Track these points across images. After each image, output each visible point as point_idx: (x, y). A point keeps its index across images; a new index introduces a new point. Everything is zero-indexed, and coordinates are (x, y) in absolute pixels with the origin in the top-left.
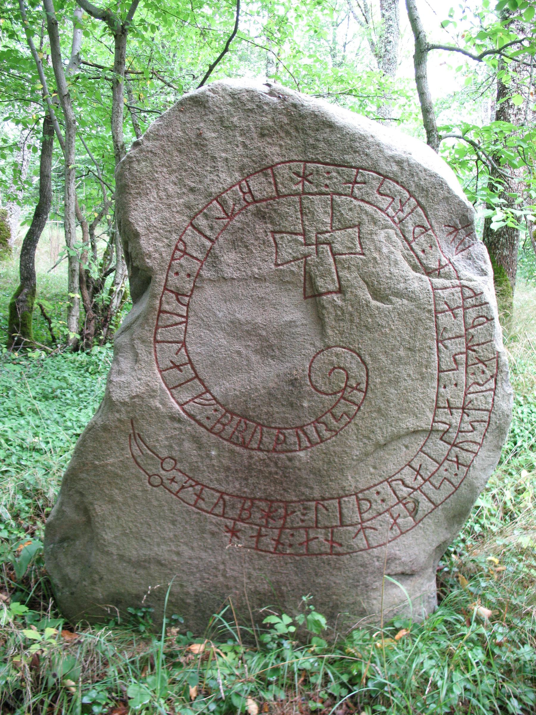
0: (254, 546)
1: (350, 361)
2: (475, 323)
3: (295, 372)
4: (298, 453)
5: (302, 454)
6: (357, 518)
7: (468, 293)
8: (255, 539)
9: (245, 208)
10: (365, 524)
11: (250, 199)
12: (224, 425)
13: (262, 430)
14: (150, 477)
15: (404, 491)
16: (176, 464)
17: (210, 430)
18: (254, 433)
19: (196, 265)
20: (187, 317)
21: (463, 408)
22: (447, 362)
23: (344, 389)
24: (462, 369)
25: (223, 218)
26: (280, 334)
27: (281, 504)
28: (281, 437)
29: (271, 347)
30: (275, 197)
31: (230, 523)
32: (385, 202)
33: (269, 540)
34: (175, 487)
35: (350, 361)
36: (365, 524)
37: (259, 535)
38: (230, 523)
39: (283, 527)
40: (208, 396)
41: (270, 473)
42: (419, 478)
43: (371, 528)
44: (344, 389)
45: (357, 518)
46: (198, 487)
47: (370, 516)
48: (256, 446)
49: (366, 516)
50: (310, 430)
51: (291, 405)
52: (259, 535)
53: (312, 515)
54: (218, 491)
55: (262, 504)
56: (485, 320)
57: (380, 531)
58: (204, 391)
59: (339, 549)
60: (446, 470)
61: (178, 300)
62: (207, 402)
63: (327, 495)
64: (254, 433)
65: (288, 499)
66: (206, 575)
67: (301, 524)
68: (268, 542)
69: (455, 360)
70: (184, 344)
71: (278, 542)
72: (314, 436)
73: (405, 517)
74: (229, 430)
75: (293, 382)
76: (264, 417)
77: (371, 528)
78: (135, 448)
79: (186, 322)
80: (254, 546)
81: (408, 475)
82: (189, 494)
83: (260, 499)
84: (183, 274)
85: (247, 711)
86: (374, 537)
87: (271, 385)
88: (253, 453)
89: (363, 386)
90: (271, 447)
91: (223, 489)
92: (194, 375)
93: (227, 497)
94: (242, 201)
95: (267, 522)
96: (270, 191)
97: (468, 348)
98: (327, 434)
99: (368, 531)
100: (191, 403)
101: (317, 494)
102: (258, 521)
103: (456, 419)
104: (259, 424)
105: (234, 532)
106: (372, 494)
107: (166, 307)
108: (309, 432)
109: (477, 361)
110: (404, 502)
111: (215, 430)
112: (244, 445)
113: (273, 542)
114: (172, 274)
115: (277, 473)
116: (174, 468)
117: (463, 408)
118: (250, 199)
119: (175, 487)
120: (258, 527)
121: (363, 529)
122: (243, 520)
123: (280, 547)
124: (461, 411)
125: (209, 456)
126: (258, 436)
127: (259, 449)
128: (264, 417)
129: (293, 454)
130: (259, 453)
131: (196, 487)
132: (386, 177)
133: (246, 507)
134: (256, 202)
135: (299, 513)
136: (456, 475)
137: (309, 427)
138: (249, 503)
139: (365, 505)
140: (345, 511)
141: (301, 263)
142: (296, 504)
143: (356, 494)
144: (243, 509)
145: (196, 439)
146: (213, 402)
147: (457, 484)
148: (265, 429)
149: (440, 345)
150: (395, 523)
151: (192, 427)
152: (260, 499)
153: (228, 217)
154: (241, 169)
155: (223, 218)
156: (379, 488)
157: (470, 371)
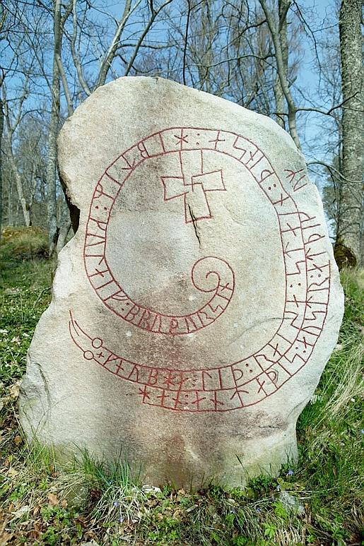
0: (160, 404)
3: (181, 276)
4: (188, 335)
5: (190, 335)
6: (232, 384)
7: (304, 217)
8: (161, 399)
9: (143, 161)
10: (239, 389)
11: (145, 155)
12: (134, 315)
13: (160, 317)
14: (85, 352)
15: (266, 364)
17: (125, 319)
18: (155, 320)
20: (105, 238)
21: (306, 302)
22: (292, 268)
25: (128, 169)
27: (177, 373)
28: (175, 323)
29: (164, 258)
30: (162, 154)
31: (142, 387)
33: (171, 400)
36: (239, 389)
38: (142, 387)
39: (179, 391)
41: (169, 349)
43: (244, 391)
45: (232, 384)
46: (119, 360)
49: (239, 383)
50: (195, 318)
51: (180, 299)
52: (164, 396)
53: (199, 381)
54: (132, 363)
55: (164, 373)
56: (318, 237)
57: (251, 394)
58: (119, 290)
61: (99, 226)
62: (121, 298)
63: (210, 366)
64: (155, 320)
65: (183, 369)
66: (127, 426)
67: (193, 388)
68: (170, 402)
70: (104, 257)
71: (177, 401)
72: (198, 323)
74: (138, 318)
76: (162, 308)
77: (244, 391)
79: (105, 242)
80: (160, 404)
81: (268, 351)
83: (162, 369)
85: (131, 438)
86: (247, 399)
88: (155, 335)
89: (231, 286)
92: (112, 279)
93: (139, 368)
94: (140, 157)
95: (168, 386)
97: (307, 257)
98: (207, 321)
99: (240, 393)
100: (111, 299)
101: (202, 366)
104: (158, 313)
105: (145, 394)
106: (242, 366)
107: (90, 231)
108: (194, 319)
111: (128, 318)
113: (174, 401)
114: (93, 207)
115: (173, 350)
116: (101, 346)
117: (306, 302)
118: (145, 155)
120: (162, 390)
121: (237, 391)
122: (151, 385)
123: (178, 404)
124: (305, 304)
125: (124, 337)
126: (158, 323)
127: (159, 332)
128: (162, 308)
129: (184, 335)
130: (161, 335)
131: (117, 360)
132: (194, 220)
133: (152, 375)
134: (149, 157)
135: (190, 379)
136: (305, 351)
137: (194, 315)
139: (238, 374)
140: (223, 378)
142: (189, 373)
144: (151, 376)
146: (126, 298)
147: (305, 359)
148: (163, 317)
149: (285, 255)
150: (261, 388)
152: (162, 369)
153: (131, 168)
154: (139, 135)
155: (128, 169)
156: (247, 361)
157: (309, 275)
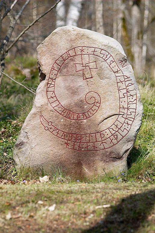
1: (95, 95)
2: (128, 85)
5: (85, 121)
6: (100, 139)
7: (126, 77)
16: (52, 124)
19: (56, 72)
20: (54, 85)
22: (122, 96)
23: (94, 103)
24: (126, 97)
26: (77, 89)
32: (102, 56)
34: (51, 130)
35: (95, 95)
37: (74, 145)
40: (60, 105)
42: (120, 81)
44: (94, 103)
45: (100, 139)
47: (104, 139)
48: (72, 119)
52: (74, 145)
54: (63, 131)
59: (97, 149)
60: (125, 126)
69: (124, 95)
72: (87, 116)
73: (114, 140)
75: (81, 101)
78: (41, 119)
82: (55, 132)
84: (53, 74)
87: (76, 102)
88: (72, 120)
89: (99, 102)
90: (76, 119)
91: (64, 131)
96: (74, 54)
101: (89, 132)
102: (74, 141)
103: (126, 111)
109: (130, 95)
110: (114, 135)
112: (69, 118)
119: (51, 130)
122: (69, 140)
127: (73, 119)
138: (71, 135)
139: (102, 136)
141: (82, 71)
143: (117, 83)
144: (69, 137)
145: (56, 116)
151: (56, 113)
156: (106, 131)
